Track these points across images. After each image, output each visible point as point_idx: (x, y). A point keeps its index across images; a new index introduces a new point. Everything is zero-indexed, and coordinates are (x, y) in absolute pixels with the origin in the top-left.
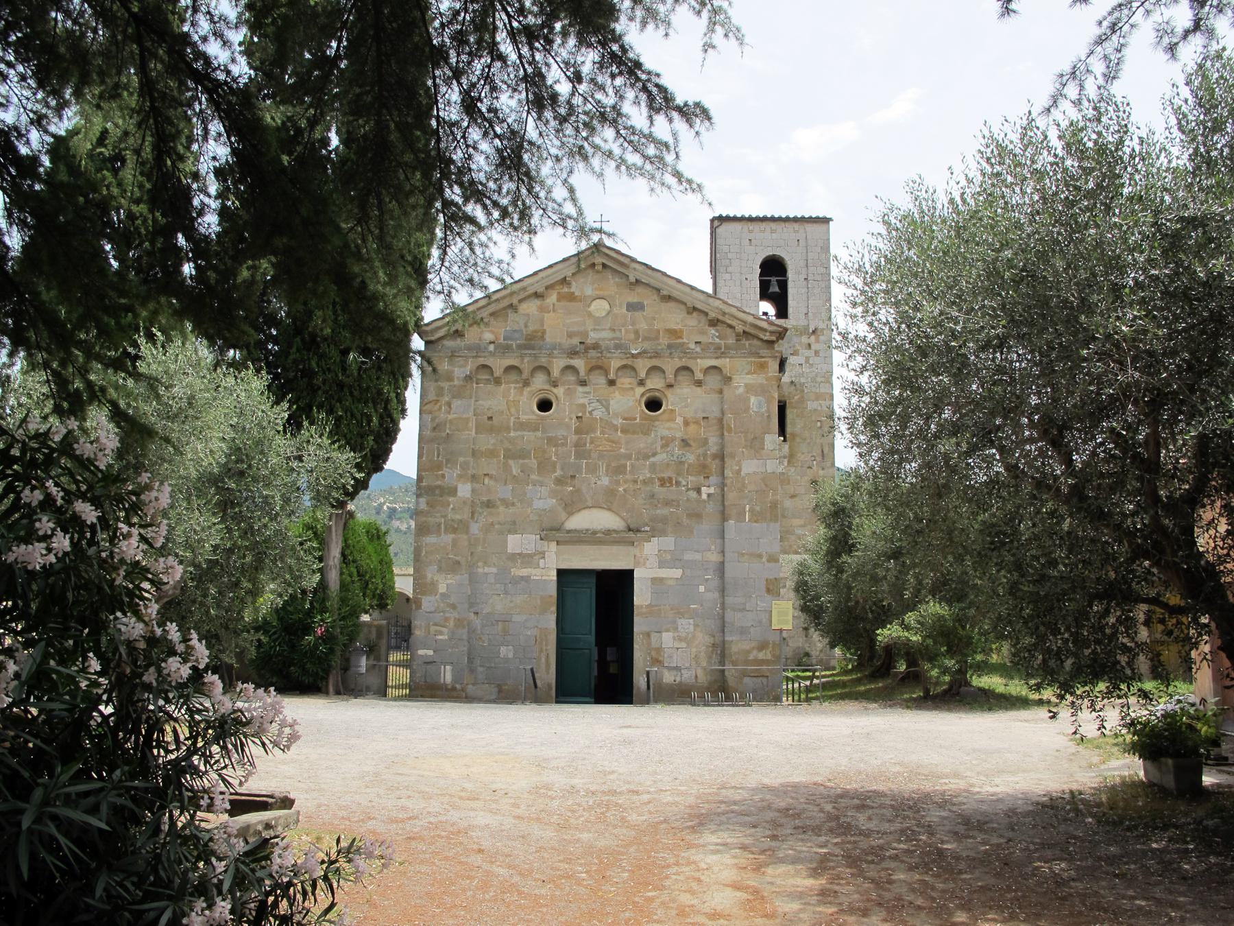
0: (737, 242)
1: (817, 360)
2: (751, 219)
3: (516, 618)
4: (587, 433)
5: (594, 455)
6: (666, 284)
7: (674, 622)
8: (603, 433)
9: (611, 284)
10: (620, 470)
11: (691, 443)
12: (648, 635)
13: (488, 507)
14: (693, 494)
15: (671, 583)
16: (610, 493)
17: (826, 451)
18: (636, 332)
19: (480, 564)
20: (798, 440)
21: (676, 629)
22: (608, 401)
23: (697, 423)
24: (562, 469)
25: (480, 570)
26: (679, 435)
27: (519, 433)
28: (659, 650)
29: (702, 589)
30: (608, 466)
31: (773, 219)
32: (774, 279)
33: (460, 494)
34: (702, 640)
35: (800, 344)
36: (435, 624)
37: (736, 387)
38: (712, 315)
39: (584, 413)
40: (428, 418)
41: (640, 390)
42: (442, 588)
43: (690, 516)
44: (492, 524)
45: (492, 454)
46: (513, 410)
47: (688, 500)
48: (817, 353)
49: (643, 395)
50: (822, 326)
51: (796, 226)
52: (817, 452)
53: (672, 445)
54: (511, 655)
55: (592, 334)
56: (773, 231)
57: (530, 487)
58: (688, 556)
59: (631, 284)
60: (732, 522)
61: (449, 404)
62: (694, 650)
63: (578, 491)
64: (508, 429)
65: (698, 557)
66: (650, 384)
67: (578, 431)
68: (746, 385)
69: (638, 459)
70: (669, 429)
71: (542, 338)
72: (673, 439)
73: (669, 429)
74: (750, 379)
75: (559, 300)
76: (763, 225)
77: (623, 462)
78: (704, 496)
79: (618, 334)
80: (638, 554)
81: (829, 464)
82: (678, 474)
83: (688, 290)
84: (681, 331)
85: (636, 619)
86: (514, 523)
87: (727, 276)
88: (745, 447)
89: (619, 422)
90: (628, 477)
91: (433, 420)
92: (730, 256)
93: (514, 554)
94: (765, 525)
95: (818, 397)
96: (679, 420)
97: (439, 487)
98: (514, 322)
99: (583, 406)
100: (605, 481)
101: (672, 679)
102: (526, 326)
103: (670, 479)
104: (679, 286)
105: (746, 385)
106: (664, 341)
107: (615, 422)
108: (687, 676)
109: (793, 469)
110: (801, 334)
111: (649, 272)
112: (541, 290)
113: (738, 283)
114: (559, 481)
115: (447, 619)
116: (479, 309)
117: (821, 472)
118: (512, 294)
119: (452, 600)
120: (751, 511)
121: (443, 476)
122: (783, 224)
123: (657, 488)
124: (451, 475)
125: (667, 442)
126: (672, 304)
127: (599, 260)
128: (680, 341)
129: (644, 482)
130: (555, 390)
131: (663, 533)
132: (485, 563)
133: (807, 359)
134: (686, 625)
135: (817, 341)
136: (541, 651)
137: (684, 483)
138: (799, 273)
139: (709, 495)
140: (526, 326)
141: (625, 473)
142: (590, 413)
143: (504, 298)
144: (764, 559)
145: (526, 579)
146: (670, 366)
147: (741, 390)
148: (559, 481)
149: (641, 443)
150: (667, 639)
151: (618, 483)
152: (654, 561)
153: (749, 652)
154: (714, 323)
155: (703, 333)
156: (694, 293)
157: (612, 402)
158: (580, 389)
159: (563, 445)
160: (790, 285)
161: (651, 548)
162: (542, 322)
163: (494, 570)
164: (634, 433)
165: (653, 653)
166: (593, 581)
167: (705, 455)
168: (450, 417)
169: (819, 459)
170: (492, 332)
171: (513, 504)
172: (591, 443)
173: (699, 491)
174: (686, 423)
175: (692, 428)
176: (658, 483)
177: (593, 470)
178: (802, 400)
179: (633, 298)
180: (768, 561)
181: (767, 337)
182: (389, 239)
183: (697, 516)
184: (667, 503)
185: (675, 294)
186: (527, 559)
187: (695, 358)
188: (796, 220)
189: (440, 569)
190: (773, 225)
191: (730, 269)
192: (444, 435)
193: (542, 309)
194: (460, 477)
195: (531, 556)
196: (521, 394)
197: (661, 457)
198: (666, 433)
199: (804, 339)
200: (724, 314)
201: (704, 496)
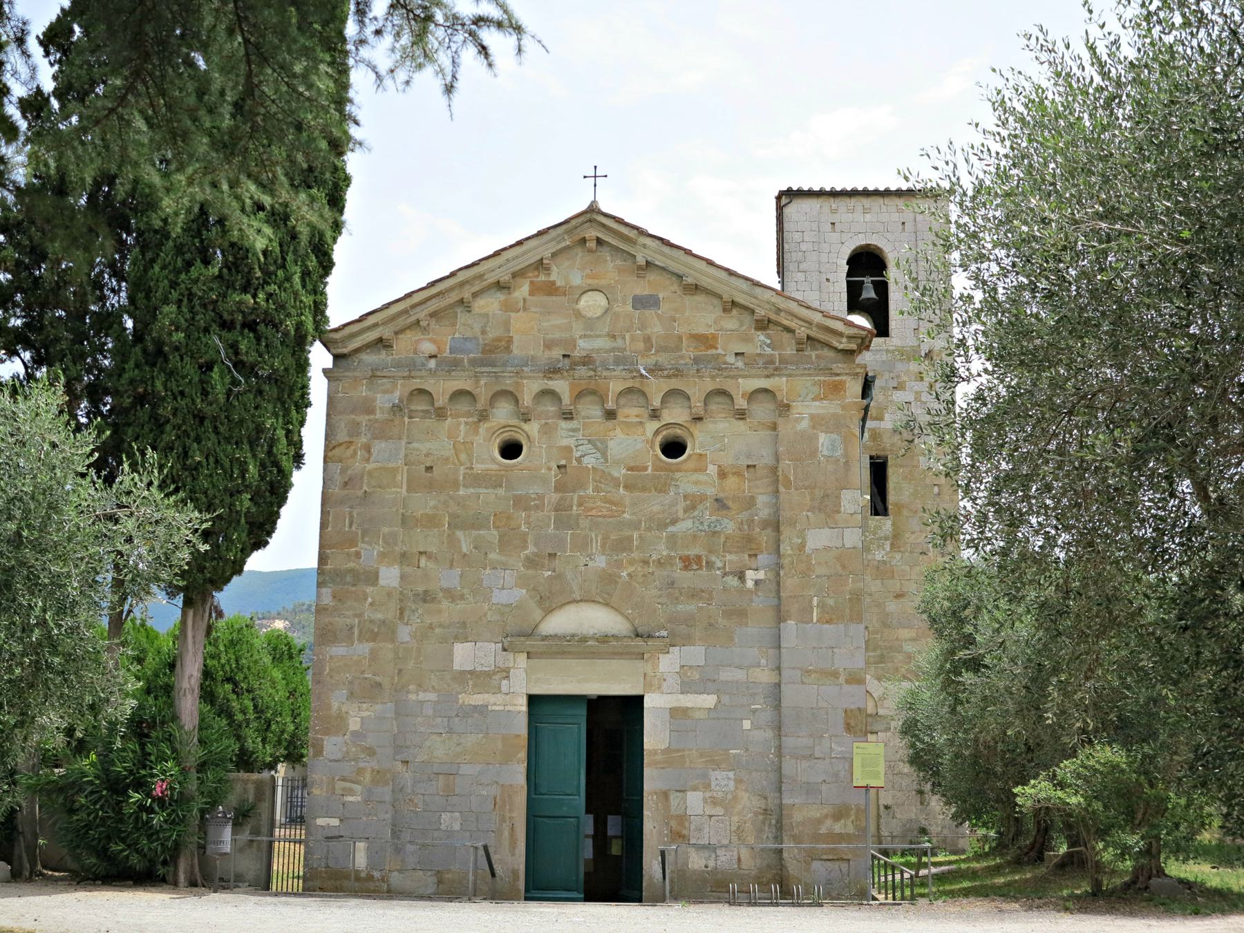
0: (815, 226)
2: (834, 194)
3: (466, 769)
4: (574, 491)
5: (584, 523)
6: (686, 265)
7: (705, 776)
8: (597, 489)
9: (610, 268)
10: (623, 545)
11: (730, 504)
12: (665, 795)
13: (425, 601)
14: (733, 581)
15: (698, 715)
16: (608, 579)
18: (647, 339)
19: (412, 687)
21: (707, 786)
22: (604, 442)
23: (738, 474)
24: (536, 545)
25: (412, 697)
26: (711, 491)
27: (472, 490)
28: (682, 818)
29: (747, 724)
30: (605, 538)
31: (866, 193)
32: (868, 280)
33: (382, 582)
34: (748, 803)
35: (907, 372)
36: (344, 779)
37: (797, 420)
38: (761, 312)
39: (569, 459)
40: (336, 468)
41: (655, 425)
42: (354, 724)
43: (728, 614)
44: (431, 627)
45: (431, 521)
46: (463, 457)
47: (725, 589)
49: (657, 432)
51: (900, 202)
53: (701, 507)
54: (457, 827)
55: (582, 343)
56: (866, 211)
57: (488, 571)
58: (726, 675)
59: (640, 268)
60: (791, 622)
61: (368, 449)
62: (735, 819)
63: (559, 577)
64: (455, 485)
65: (740, 675)
66: (668, 417)
67: (559, 488)
68: (812, 417)
69: (649, 529)
70: (696, 483)
71: (508, 349)
72: (703, 498)
73: (696, 483)
74: (819, 408)
75: (532, 293)
76: (852, 202)
77: (627, 533)
78: (750, 584)
79: (619, 343)
80: (650, 673)
82: (710, 551)
83: (724, 275)
84: (715, 337)
85: (647, 772)
86: (464, 625)
88: (812, 509)
89: (620, 472)
90: (636, 555)
91: (343, 471)
92: (804, 247)
93: (463, 673)
94: (841, 627)
96: (712, 470)
97: (351, 571)
98: (467, 326)
99: (568, 449)
100: (600, 562)
101: (702, 863)
102: (484, 332)
103: (699, 558)
104: (711, 270)
105: (812, 417)
106: (689, 352)
107: (616, 474)
108: (725, 860)
110: (909, 360)
111: (667, 250)
112: (505, 277)
113: (815, 285)
114: (531, 563)
115: (360, 771)
116: (414, 306)
118: (462, 284)
119: (370, 741)
120: (822, 605)
121: (358, 555)
122: (880, 200)
123: (678, 573)
124: (370, 553)
125: (693, 503)
126: (700, 298)
127: (592, 233)
128: (713, 352)
129: (659, 563)
130: (526, 427)
131: (687, 640)
132: (420, 685)
134: (722, 780)
136: (503, 820)
137: (719, 564)
139: (757, 582)
140: (484, 332)
141: (631, 550)
142: (579, 460)
143: (451, 289)
144: (842, 679)
145: (481, 710)
146: (697, 389)
147: (804, 424)
148: (531, 563)
149: (655, 504)
150: (695, 801)
151: (619, 564)
152: (673, 682)
153: (819, 822)
154: (763, 325)
155: (746, 339)
156: (733, 279)
157: (611, 444)
158: (564, 424)
159: (537, 507)
161: (668, 663)
162: (507, 325)
163: (433, 696)
164: (644, 489)
165: (673, 823)
166: (582, 712)
167: (751, 522)
168: (369, 467)
170: (433, 341)
171: (462, 597)
172: (580, 505)
173: (741, 577)
174: (722, 474)
175: (731, 481)
176: (680, 565)
177: (583, 545)
179: (642, 288)
180: (848, 682)
181: (843, 344)
183: (739, 614)
184: (694, 594)
185: (705, 282)
186: (481, 679)
187: (735, 377)
189: (351, 695)
190: (866, 202)
191: (802, 267)
192: (360, 493)
193: (508, 307)
194: (383, 555)
195: (488, 675)
196: (476, 433)
197: (685, 526)
198: (692, 489)
199: (914, 367)
200: (778, 311)
201: (750, 584)
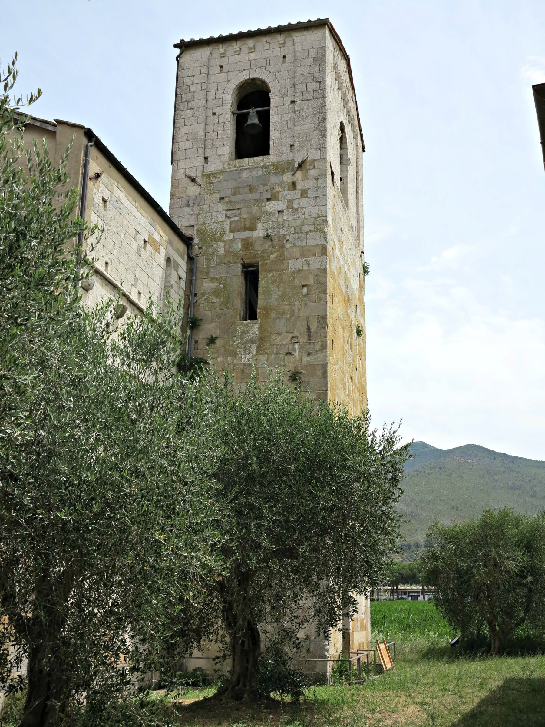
0: (204, 70)
1: (304, 202)
17: (314, 326)
20: (273, 315)
32: (252, 111)
35: (281, 184)
48: (304, 193)
50: (313, 155)
51: (280, 38)
52: (300, 330)
76: (236, 45)
81: (317, 347)
87: (189, 113)
95: (304, 253)
109: (263, 358)
113: (201, 118)
117: (306, 359)
133: (290, 203)
135: (306, 177)
138: (284, 95)
160: (273, 119)
169: (303, 340)
178: (281, 259)
182: (414, 705)
188: (280, 30)
190: (250, 43)
191: (191, 105)
199: (287, 178)
